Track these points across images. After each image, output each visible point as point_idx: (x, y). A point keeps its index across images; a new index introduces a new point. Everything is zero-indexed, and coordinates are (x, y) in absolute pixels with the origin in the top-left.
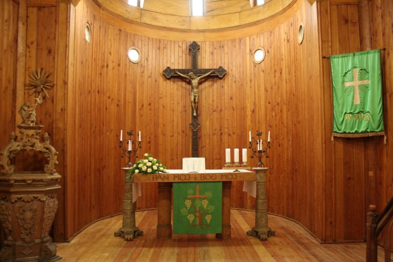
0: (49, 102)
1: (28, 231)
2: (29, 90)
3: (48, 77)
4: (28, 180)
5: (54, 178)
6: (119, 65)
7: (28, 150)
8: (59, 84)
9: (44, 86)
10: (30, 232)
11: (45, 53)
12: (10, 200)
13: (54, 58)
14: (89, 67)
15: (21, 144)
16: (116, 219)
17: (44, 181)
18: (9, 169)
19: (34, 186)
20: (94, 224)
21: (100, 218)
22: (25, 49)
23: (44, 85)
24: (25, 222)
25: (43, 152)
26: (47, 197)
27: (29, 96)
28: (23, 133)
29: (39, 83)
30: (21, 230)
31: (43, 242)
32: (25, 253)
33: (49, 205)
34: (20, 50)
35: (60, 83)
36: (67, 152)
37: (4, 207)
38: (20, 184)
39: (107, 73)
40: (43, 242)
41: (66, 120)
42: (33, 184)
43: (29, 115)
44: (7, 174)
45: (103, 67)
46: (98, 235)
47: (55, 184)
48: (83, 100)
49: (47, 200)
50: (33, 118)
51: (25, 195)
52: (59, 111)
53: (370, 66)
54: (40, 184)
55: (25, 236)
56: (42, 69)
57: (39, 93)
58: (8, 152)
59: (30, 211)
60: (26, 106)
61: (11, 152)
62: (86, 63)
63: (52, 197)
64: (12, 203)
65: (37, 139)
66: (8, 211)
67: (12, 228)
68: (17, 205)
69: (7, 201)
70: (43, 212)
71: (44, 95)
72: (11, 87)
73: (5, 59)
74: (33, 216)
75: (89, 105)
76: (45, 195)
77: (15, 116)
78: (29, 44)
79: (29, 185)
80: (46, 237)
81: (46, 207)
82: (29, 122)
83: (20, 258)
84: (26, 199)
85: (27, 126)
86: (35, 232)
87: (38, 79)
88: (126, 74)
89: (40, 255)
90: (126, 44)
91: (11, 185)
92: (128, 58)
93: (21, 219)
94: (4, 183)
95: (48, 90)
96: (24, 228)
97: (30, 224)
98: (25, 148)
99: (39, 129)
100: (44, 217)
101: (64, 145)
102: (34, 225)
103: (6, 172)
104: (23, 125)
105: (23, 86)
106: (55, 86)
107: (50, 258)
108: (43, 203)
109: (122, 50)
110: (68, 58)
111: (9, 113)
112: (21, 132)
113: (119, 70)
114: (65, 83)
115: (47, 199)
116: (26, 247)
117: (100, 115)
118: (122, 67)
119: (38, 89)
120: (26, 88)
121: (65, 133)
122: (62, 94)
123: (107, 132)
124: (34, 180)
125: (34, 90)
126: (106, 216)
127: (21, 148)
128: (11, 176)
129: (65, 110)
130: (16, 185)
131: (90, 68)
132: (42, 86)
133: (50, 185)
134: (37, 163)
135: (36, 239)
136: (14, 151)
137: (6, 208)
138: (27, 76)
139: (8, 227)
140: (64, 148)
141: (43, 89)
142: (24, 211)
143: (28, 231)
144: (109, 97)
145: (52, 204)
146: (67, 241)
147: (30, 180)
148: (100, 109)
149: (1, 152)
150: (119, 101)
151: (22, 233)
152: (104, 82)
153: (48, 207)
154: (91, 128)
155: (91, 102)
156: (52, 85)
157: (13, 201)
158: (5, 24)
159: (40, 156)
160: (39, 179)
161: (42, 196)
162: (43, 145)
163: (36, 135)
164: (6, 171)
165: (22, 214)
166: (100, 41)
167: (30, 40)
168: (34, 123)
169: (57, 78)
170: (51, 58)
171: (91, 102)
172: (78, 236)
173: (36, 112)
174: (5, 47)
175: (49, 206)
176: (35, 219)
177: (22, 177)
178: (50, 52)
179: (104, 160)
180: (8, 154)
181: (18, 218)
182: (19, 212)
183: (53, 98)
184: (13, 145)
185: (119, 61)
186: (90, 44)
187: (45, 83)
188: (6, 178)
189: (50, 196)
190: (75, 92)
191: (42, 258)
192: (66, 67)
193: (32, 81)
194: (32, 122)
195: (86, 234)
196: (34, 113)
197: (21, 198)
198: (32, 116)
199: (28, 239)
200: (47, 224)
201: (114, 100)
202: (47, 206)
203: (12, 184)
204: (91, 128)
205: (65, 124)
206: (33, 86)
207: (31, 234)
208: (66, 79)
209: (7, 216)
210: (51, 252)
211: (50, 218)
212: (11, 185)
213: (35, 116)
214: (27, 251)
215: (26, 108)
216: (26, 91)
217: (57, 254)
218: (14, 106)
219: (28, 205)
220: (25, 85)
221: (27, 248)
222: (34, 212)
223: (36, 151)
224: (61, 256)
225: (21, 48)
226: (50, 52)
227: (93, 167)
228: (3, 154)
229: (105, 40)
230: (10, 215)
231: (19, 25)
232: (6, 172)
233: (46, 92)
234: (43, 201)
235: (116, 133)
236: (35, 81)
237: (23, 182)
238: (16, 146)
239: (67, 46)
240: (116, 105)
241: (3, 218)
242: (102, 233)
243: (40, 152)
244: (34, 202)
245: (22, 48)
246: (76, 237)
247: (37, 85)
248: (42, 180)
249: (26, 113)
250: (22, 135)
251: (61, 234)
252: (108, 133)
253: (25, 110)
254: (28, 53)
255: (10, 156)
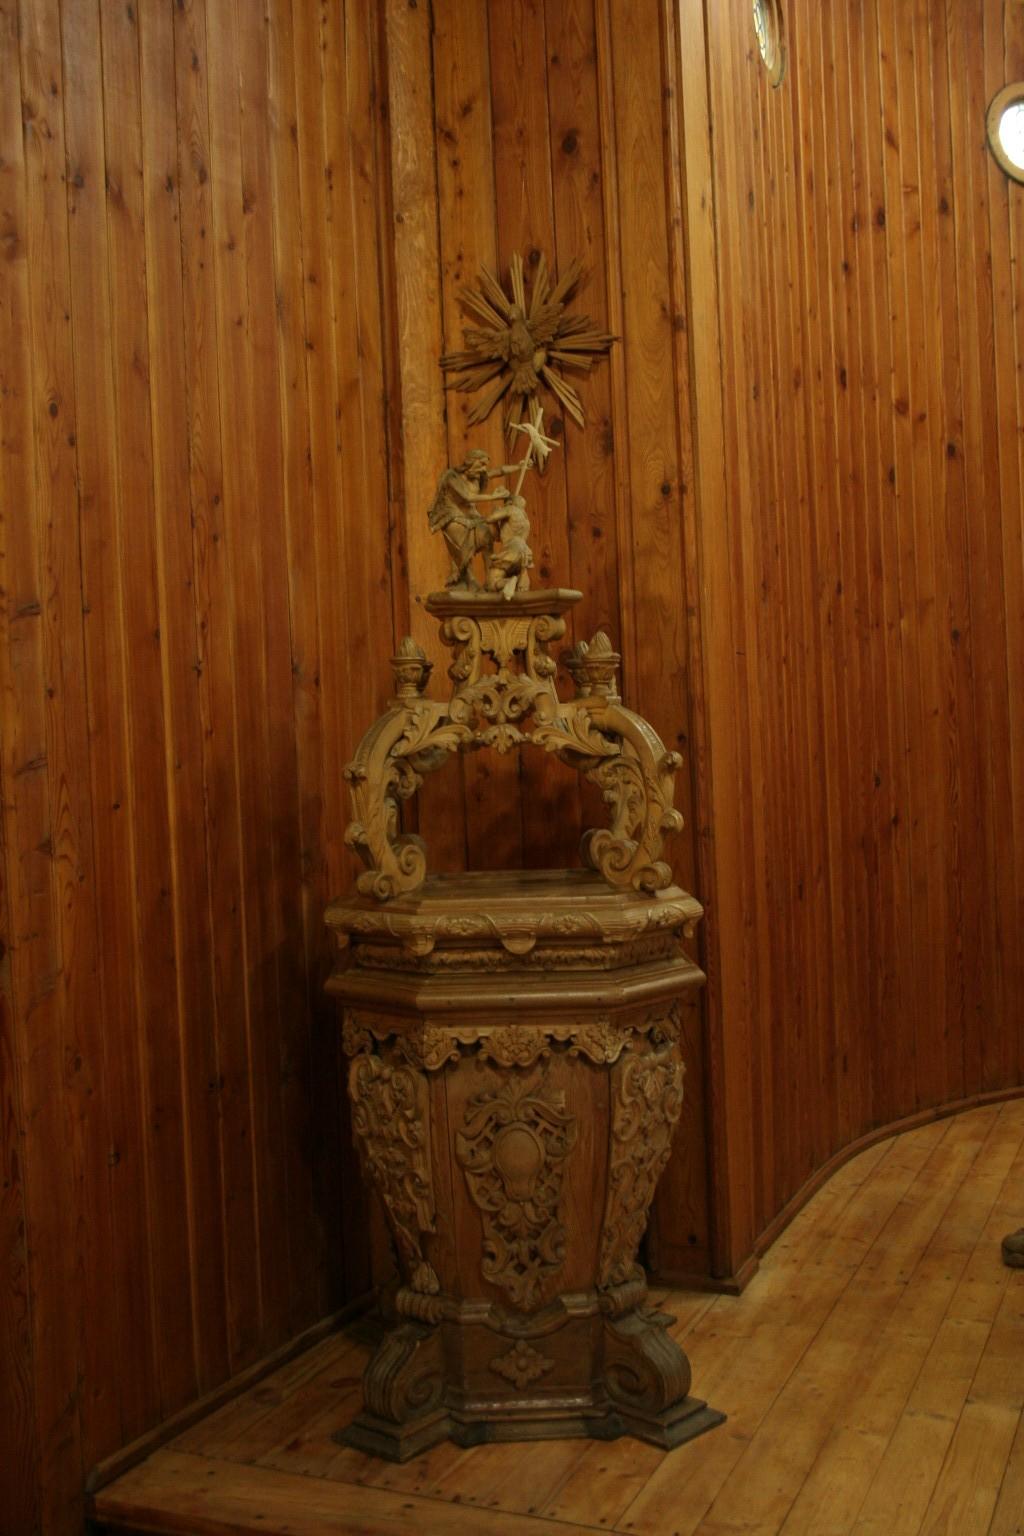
0: (586, 450)
1: (522, 1247)
2: (468, 391)
3: (568, 298)
4: (511, 936)
5: (666, 917)
6: (944, 208)
7: (503, 745)
8: (635, 334)
9: (552, 354)
10: (534, 1254)
11: (542, 153)
12: (418, 1056)
13: (597, 179)
14: (783, 226)
15: (458, 710)
16: (974, 1136)
17: (607, 940)
18: (401, 866)
19: (549, 972)
20: (851, 1164)
21: (877, 1124)
22: (429, 154)
23: (549, 347)
24: (503, 1187)
25: (588, 757)
26: (625, 1038)
27: (470, 426)
28: (466, 642)
29: (521, 337)
30: (484, 1238)
31: (608, 1315)
32: (511, 1371)
33: (641, 1089)
34: (405, 160)
35: (642, 324)
36: (708, 748)
37: (385, 1093)
38: (467, 957)
39: (881, 261)
40: (608, 1315)
41: (691, 550)
42: (539, 961)
43: (492, 528)
44: (387, 899)
45: (855, 223)
46: (901, 1248)
47: (669, 958)
48: (770, 431)
49: (627, 1057)
50: (517, 546)
51: (501, 1030)
52: (650, 497)
53: (238, 730)
54: (583, 958)
55: (510, 1272)
56: (532, 259)
57: (526, 399)
58: (391, 761)
59: (534, 1124)
60: (471, 479)
61: (403, 763)
62: (769, 202)
63: (654, 1041)
64: (425, 1072)
65: (543, 674)
66: (408, 1121)
67: (435, 1220)
68: (458, 1086)
69: (402, 1060)
70: (609, 1135)
71: (558, 412)
72: (374, 382)
73: (329, 219)
74: (549, 1158)
75: (800, 455)
76: (617, 1026)
77: (402, 551)
78: (452, 122)
79: (519, 967)
80: (625, 1282)
81: (623, 1105)
82: (497, 575)
83: (482, 1398)
84: (505, 1053)
85: (485, 596)
86: (562, 1251)
87: (514, 315)
88: (989, 258)
89: (596, 1391)
90: (978, 75)
91: (418, 968)
92: (994, 155)
93: (481, 1175)
94: (378, 951)
95: (572, 379)
96: (500, 1228)
97: (536, 1206)
98: (481, 736)
99: (556, 616)
100: (614, 1164)
101: (691, 705)
102: (554, 1212)
103: (384, 884)
104: (460, 594)
105: (437, 371)
106: (616, 349)
107: (658, 1421)
108: (602, 1077)
109: (956, 115)
110: (682, 164)
111: (373, 533)
112: (452, 641)
113: (944, 239)
114: (676, 323)
115: (625, 1049)
116: (517, 1338)
117: (859, 514)
118: (964, 217)
119: (521, 374)
120: (453, 378)
121: (694, 632)
122: (657, 396)
123: (901, 616)
124: (547, 938)
125: (496, 386)
126: (911, 1113)
127: (460, 735)
128: (413, 913)
129: (682, 489)
130: (442, 964)
131: (791, 228)
132: (540, 357)
133: (639, 964)
134: (534, 820)
135: (571, 1292)
136: (423, 754)
137: (397, 1103)
138: (454, 311)
139: (414, 1215)
140: (690, 723)
141: (548, 372)
142: (498, 1126)
143: (522, 1247)
144: (902, 407)
145: (655, 1076)
146: (728, 1282)
147: (525, 935)
148: (856, 477)
149: (352, 766)
150: (957, 425)
151: (492, 1256)
152: (866, 312)
153: (634, 1104)
154: (817, 595)
155: (807, 437)
156: (600, 347)
157: (434, 1062)
158: (321, 12)
159: (554, 775)
160: (575, 929)
161: (595, 1034)
162: (584, 712)
163: (536, 654)
164: (388, 878)
165: (488, 1143)
166: (829, 68)
167: (454, 92)
168: (525, 578)
169: (623, 295)
170: (582, 180)
171: (807, 437)
172: (776, 1251)
173: (530, 512)
174: (327, 153)
175: (639, 1099)
176: (560, 1177)
177: (477, 916)
178: (569, 144)
179: (893, 783)
180: (392, 775)
181: (463, 1167)
182: (470, 1131)
183: (607, 423)
184: (416, 719)
185: (941, 182)
186: (781, 87)
187: (559, 336)
188: (390, 920)
189: (643, 1029)
190: (731, 378)
191: (611, 1410)
192: (674, 226)
193: (482, 336)
194: (513, 571)
195: (826, 1235)
196: (518, 513)
197: (477, 1046)
198: (506, 533)
199: (523, 1290)
200: (631, 1202)
201: (927, 420)
202: (630, 1094)
203: (422, 960)
204: (817, 595)
205: (689, 575)
206: (489, 361)
207: (538, 1261)
208: (679, 300)
209: (408, 1152)
210: (658, 1379)
211: (649, 1166)
212: (418, 968)
213: (526, 534)
214: (523, 1363)
215: (470, 491)
216: (452, 395)
217: (697, 1393)
218: (395, 494)
219: (519, 1087)
220: (445, 366)
221: (521, 1345)
222: (557, 1132)
223: (547, 749)
224: (713, 1404)
225: (409, 151)
226: (569, 144)
227: (834, 824)
228: (364, 778)
229: (855, 59)
230: (421, 1148)
231: (387, 15)
232: (384, 884)
233: (563, 388)
234: (606, 1067)
235: (951, 620)
236: (497, 330)
237: (484, 949)
238: (428, 724)
239: (667, 93)
240: (944, 448)
241: (386, 1161)
242: (920, 1227)
243: (571, 755)
244: (551, 1068)
245: (412, 151)
246: (768, 1256)
247: (511, 356)
248: (593, 938)
249: (471, 517)
250: (455, 656)
251: (693, 1239)
252: (904, 623)
253: (464, 504)
254: (447, 173)
255: (401, 790)
